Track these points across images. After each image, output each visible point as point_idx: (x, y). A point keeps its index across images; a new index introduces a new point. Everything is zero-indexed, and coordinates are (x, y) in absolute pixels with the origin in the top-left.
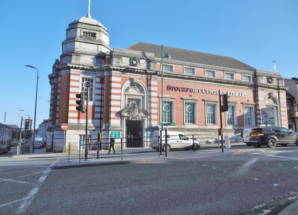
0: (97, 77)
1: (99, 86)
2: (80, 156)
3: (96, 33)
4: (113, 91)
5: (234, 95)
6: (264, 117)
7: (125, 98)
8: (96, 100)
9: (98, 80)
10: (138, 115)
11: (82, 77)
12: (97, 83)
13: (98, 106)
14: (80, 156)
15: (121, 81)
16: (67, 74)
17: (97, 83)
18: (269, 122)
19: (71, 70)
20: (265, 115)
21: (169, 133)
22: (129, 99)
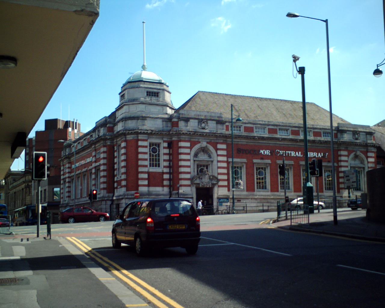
0: (164, 141)
1: (167, 151)
2: (129, 109)
3: (159, 92)
4: (4, 228)
5: (312, 156)
6: (347, 180)
7: (194, 164)
8: (164, 167)
9: (166, 145)
10: (205, 181)
11: (150, 142)
12: (164, 148)
13: (166, 173)
14: (129, 109)
15: (46, 225)
16: (135, 139)
17: (164, 148)
18: (351, 187)
19: (139, 135)
20: (347, 178)
21: (301, 219)
22: (198, 165)
